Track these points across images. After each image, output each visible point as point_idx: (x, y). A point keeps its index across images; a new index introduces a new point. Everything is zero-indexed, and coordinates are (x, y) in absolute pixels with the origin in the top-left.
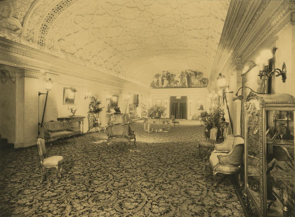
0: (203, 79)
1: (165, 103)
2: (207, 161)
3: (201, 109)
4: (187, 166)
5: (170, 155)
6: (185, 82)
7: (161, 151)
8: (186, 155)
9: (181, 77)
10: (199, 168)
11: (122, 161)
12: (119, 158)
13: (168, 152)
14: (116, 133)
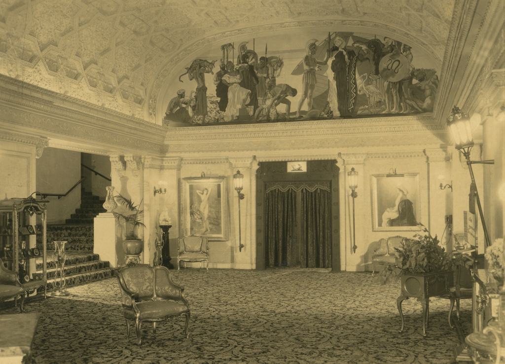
0: (413, 75)
1: (236, 193)
3: (405, 221)
4: (369, 353)
5: (325, 332)
6: (327, 93)
7: (301, 322)
8: (365, 332)
9: (306, 68)
10: (398, 358)
11: (207, 344)
12: (198, 339)
13: (300, 351)
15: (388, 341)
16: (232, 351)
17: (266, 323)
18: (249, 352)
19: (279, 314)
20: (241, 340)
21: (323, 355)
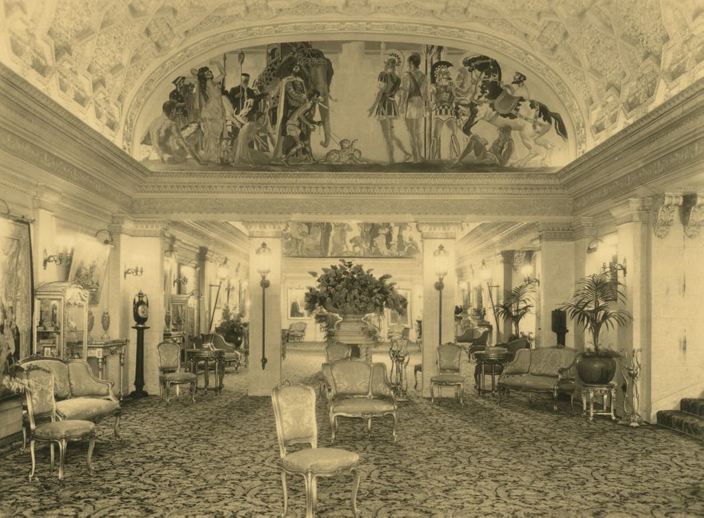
2: (231, 514)
14: (346, 384)
15: (412, 495)
16: (94, 509)
17: (141, 475)
18: (67, 509)
19: (156, 461)
20: (135, 484)
21: (254, 474)
